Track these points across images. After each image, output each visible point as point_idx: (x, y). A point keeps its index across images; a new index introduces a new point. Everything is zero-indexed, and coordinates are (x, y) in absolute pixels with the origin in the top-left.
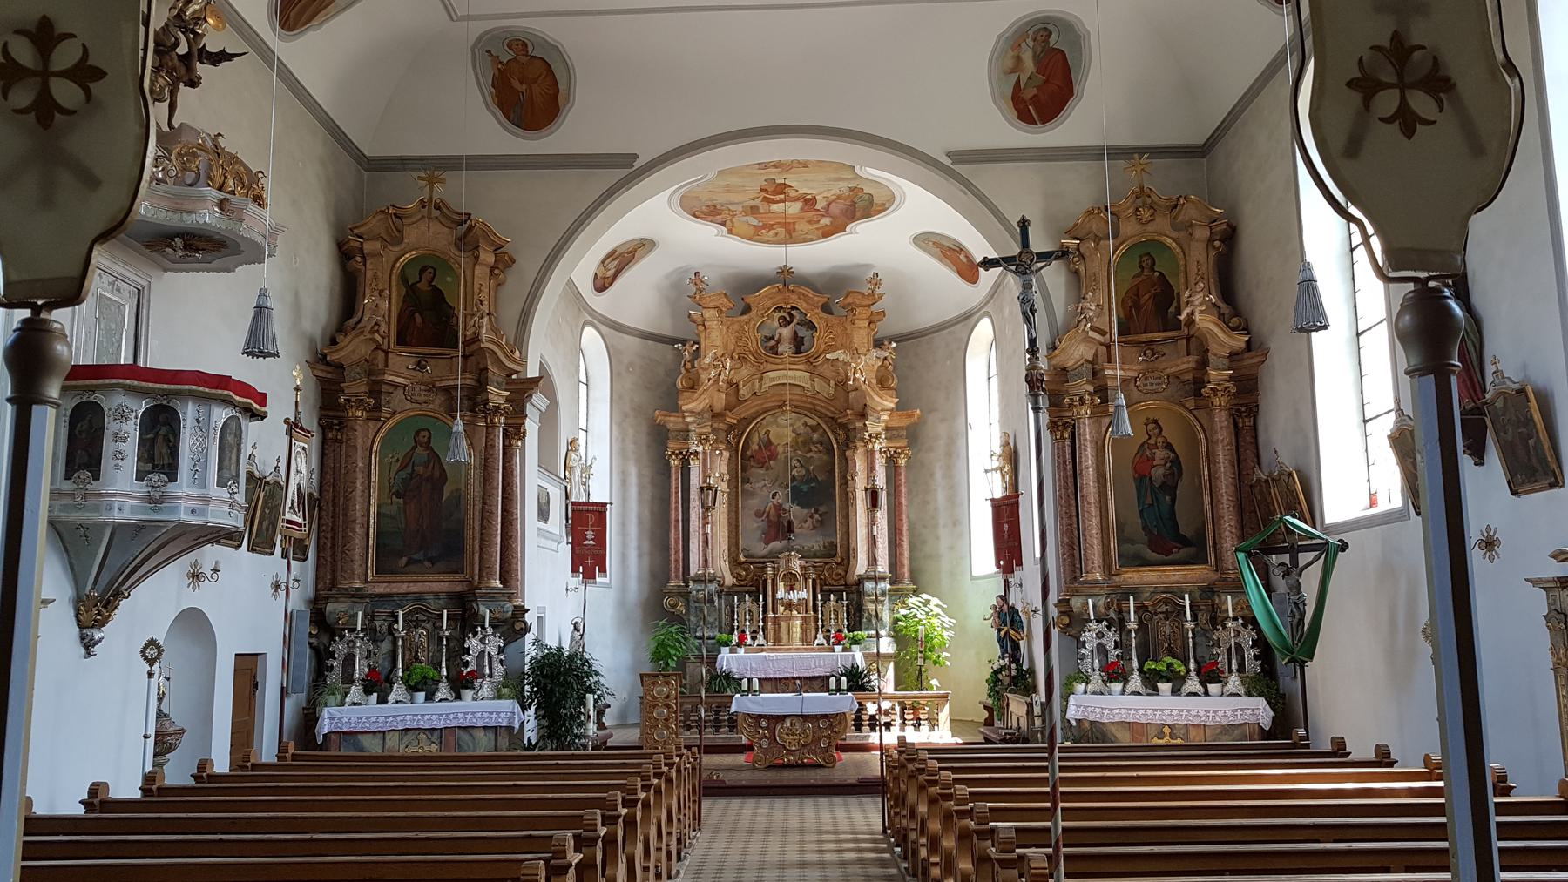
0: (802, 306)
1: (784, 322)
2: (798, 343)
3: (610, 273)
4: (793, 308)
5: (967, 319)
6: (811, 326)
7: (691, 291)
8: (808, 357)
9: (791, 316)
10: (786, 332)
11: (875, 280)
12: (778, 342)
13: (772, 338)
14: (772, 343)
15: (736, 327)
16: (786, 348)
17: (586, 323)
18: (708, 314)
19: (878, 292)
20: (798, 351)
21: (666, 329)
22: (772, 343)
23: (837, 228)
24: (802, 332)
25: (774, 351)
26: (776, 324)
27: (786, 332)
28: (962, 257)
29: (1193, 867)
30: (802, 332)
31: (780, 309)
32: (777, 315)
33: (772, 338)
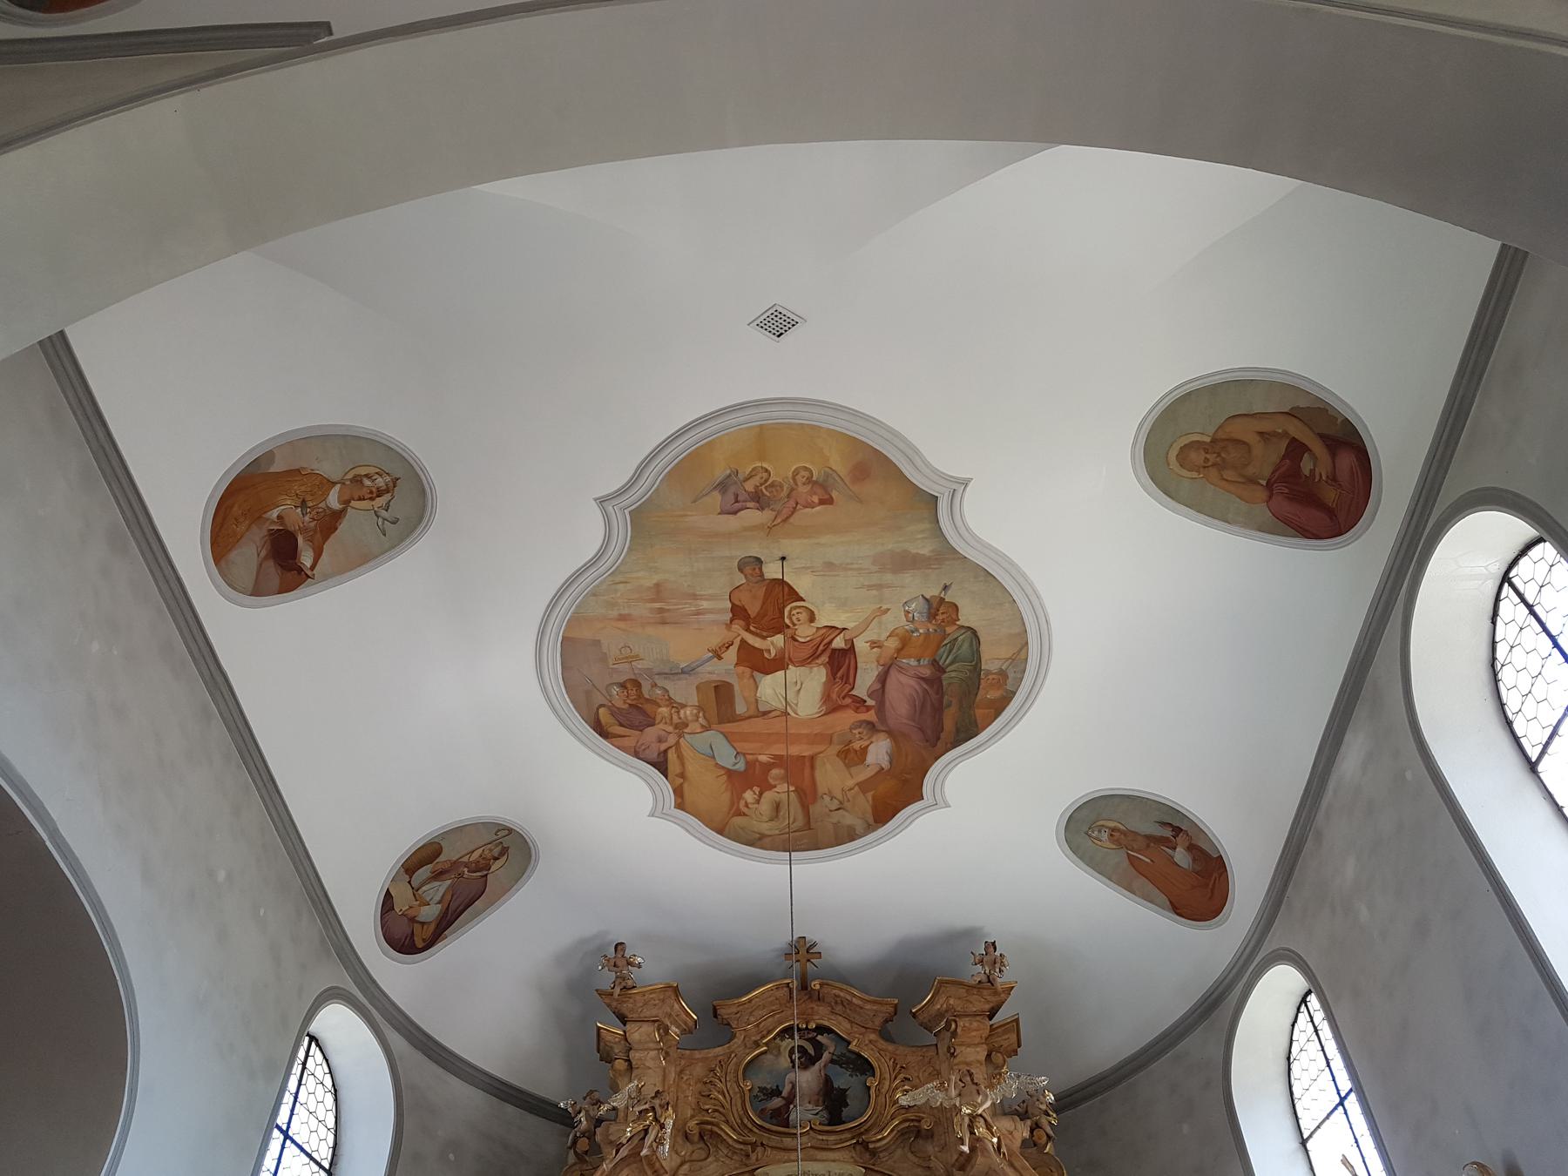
0: (841, 1026)
1: (808, 1061)
2: (833, 1103)
3: (430, 913)
4: (822, 1029)
5: (1218, 1007)
6: (863, 1066)
7: (602, 990)
8: (858, 1132)
9: (819, 1047)
10: (807, 1080)
11: (991, 956)
12: (790, 1100)
13: (777, 1092)
14: (777, 1102)
15: (699, 1070)
16: (803, 1112)
17: (332, 995)
18: (637, 1033)
19: (1001, 981)
20: (835, 1118)
21: (551, 1084)
22: (777, 1102)
23: (896, 794)
24: (843, 1079)
25: (781, 1117)
26: (784, 1062)
27: (807, 1080)
28: (1181, 856)
29: (280, 808)
30: (843, 1079)
31: (788, 1032)
32: (786, 1044)
33: (777, 1092)
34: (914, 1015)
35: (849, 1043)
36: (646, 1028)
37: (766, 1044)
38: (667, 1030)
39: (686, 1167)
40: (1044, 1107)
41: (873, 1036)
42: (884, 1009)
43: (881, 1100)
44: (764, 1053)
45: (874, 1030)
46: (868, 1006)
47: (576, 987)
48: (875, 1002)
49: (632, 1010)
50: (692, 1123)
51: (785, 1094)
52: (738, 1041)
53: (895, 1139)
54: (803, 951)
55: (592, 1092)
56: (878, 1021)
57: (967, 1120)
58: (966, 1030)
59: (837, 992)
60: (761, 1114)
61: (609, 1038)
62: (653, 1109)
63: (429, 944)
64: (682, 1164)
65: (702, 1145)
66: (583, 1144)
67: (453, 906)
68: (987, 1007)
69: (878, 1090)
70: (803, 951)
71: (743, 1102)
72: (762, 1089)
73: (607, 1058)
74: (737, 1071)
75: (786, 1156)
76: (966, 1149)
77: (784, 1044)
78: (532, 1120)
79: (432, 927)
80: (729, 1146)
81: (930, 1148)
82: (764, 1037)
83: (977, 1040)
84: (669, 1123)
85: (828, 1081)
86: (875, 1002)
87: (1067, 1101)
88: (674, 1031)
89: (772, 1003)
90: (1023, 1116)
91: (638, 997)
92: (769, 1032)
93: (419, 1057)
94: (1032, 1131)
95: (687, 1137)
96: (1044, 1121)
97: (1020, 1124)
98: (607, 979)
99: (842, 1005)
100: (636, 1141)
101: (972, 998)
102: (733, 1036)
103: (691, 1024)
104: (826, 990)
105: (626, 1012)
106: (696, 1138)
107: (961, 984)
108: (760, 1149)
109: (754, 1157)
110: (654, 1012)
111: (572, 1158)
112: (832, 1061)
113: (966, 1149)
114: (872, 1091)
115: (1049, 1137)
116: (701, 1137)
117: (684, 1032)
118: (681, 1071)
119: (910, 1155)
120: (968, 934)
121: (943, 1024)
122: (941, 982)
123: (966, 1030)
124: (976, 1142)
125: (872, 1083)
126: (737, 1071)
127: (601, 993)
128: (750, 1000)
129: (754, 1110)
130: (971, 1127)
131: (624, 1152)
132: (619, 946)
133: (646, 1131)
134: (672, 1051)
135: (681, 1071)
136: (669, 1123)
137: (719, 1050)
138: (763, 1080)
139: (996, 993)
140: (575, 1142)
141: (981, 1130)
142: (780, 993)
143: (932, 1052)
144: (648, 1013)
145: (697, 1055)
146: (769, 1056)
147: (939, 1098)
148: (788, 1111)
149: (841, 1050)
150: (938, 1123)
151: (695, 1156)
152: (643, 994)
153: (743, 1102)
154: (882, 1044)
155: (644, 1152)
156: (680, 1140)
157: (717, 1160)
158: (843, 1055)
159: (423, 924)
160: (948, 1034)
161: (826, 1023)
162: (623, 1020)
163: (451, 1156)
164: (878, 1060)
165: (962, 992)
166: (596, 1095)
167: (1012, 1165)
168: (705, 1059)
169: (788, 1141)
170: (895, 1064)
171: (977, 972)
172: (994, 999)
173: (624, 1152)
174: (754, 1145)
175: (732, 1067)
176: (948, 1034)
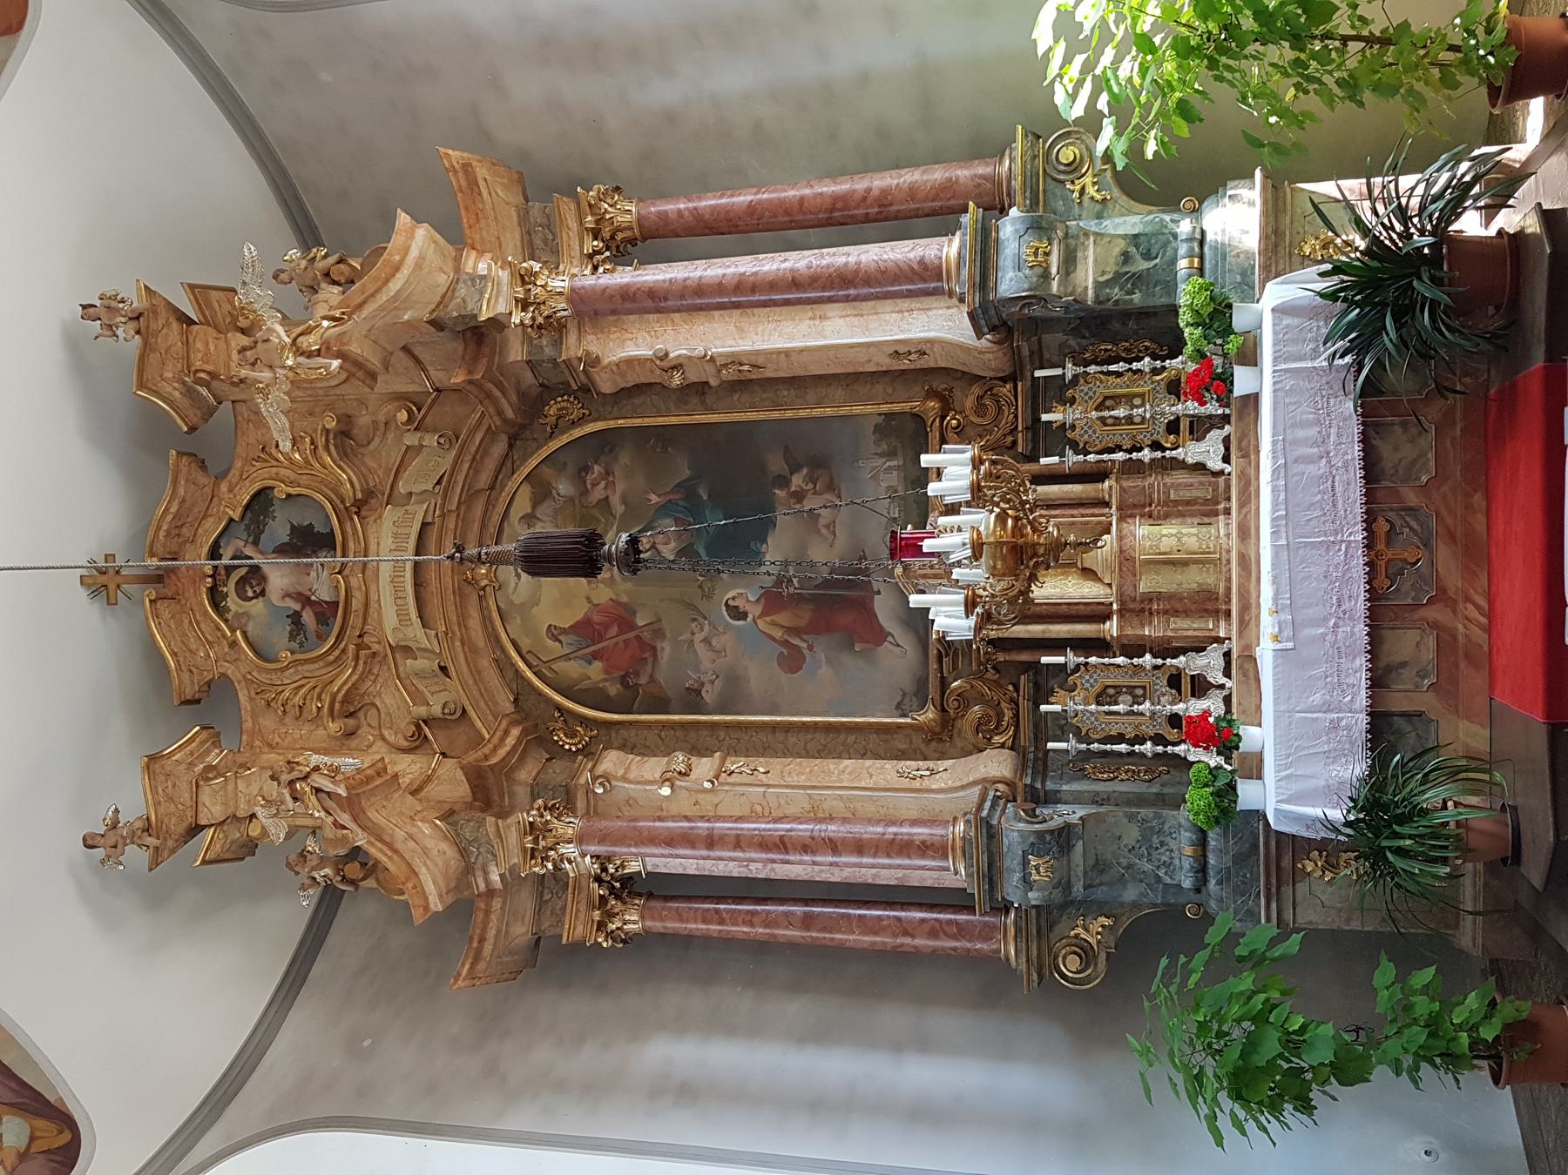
2: (309, 541)
6: (261, 502)
10: (279, 576)
12: (306, 601)
13: (296, 618)
14: (308, 617)
15: (268, 722)
18: (212, 808)
19: (137, 302)
22: (308, 617)
24: (278, 529)
25: (326, 611)
26: (257, 607)
27: (279, 576)
30: (278, 529)
32: (233, 603)
33: (296, 618)
34: (192, 429)
35: (232, 520)
36: (205, 797)
37: (233, 631)
38: (209, 768)
39: (386, 733)
40: (304, 263)
41: (224, 487)
42: (184, 470)
43: (304, 480)
44: (245, 634)
45: (216, 485)
46: (181, 491)
47: (156, 899)
48: (175, 482)
49: (181, 818)
50: (333, 727)
51: (297, 607)
52: (230, 670)
53: (352, 465)
54: (103, 579)
55: (288, 865)
56: (202, 479)
57: (301, 359)
58: (206, 358)
59: (162, 534)
60: (322, 638)
61: (217, 847)
62: (291, 783)
63: (66, 1121)
64: (384, 739)
65: (361, 715)
66: (353, 870)
67: (9, 1097)
68: (175, 325)
69: (291, 483)
70: (103, 579)
71: (306, 661)
72: (292, 637)
73: (249, 848)
74: (269, 671)
75: (373, 605)
76: (336, 363)
77: (233, 607)
78: (333, 940)
79: (41, 1123)
80: (362, 679)
81: (364, 420)
82: (224, 636)
83: (222, 345)
84: (316, 759)
85: (281, 550)
86: (175, 482)
87: (308, 235)
88: (214, 759)
89: (180, 624)
90: (314, 290)
91: (162, 810)
92: (218, 629)
93: (232, 1111)
94: (334, 283)
95: (350, 734)
96: (321, 265)
97: (321, 296)
98: (135, 856)
99: (179, 530)
100: (330, 804)
101: (162, 346)
102: (223, 675)
103: (205, 734)
104: (159, 549)
105: (185, 824)
106: (351, 722)
107: (142, 358)
108: (366, 639)
109: (375, 647)
110: (183, 785)
111: (371, 883)
112: (256, 543)
113: (336, 363)
114: (293, 491)
115: (340, 261)
116: (351, 715)
117: (217, 744)
118: (270, 745)
119: (371, 447)
120: (73, 345)
121: (204, 391)
122: (142, 385)
123: (206, 358)
124: (325, 350)
125: (281, 491)
126: (269, 671)
127: (155, 862)
128: (174, 654)
129: (322, 645)
130: (310, 355)
131: (345, 819)
132: (89, 843)
133: (318, 790)
134: (240, 759)
135: (270, 745)
136: (316, 759)
137: (243, 696)
138: (279, 638)
139: (154, 310)
140: (353, 882)
141: (311, 342)
142: (166, 615)
143: (241, 408)
144: (186, 797)
145: (248, 724)
146: (250, 628)
147: (278, 395)
148: (319, 603)
149: (240, 530)
150: (331, 407)
151: (375, 723)
152: (157, 804)
153: (306, 661)
154: (234, 475)
155: (342, 791)
156: (354, 743)
157: (379, 693)
158: (248, 528)
159: (32, 1139)
160: (215, 384)
161: (206, 549)
162: (196, 829)
163: (366, 1043)
164: (253, 482)
165: (153, 358)
166: (293, 857)
167: (360, 306)
168: (254, 716)
169: (356, 604)
170: (258, 459)
171: (129, 343)
172: (163, 313)
173: (345, 819)
174: (359, 647)
175: (263, 678)
176: (215, 384)
